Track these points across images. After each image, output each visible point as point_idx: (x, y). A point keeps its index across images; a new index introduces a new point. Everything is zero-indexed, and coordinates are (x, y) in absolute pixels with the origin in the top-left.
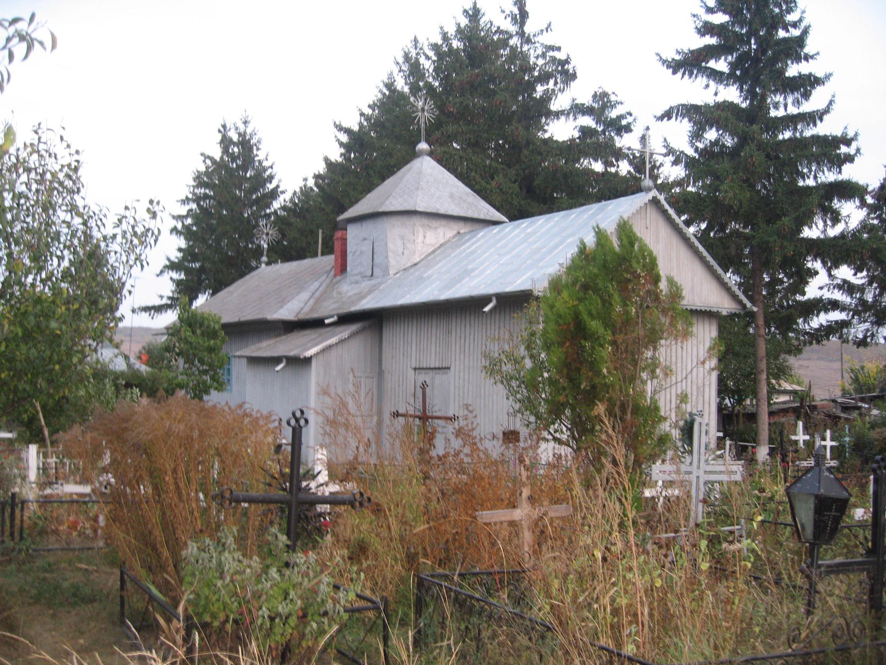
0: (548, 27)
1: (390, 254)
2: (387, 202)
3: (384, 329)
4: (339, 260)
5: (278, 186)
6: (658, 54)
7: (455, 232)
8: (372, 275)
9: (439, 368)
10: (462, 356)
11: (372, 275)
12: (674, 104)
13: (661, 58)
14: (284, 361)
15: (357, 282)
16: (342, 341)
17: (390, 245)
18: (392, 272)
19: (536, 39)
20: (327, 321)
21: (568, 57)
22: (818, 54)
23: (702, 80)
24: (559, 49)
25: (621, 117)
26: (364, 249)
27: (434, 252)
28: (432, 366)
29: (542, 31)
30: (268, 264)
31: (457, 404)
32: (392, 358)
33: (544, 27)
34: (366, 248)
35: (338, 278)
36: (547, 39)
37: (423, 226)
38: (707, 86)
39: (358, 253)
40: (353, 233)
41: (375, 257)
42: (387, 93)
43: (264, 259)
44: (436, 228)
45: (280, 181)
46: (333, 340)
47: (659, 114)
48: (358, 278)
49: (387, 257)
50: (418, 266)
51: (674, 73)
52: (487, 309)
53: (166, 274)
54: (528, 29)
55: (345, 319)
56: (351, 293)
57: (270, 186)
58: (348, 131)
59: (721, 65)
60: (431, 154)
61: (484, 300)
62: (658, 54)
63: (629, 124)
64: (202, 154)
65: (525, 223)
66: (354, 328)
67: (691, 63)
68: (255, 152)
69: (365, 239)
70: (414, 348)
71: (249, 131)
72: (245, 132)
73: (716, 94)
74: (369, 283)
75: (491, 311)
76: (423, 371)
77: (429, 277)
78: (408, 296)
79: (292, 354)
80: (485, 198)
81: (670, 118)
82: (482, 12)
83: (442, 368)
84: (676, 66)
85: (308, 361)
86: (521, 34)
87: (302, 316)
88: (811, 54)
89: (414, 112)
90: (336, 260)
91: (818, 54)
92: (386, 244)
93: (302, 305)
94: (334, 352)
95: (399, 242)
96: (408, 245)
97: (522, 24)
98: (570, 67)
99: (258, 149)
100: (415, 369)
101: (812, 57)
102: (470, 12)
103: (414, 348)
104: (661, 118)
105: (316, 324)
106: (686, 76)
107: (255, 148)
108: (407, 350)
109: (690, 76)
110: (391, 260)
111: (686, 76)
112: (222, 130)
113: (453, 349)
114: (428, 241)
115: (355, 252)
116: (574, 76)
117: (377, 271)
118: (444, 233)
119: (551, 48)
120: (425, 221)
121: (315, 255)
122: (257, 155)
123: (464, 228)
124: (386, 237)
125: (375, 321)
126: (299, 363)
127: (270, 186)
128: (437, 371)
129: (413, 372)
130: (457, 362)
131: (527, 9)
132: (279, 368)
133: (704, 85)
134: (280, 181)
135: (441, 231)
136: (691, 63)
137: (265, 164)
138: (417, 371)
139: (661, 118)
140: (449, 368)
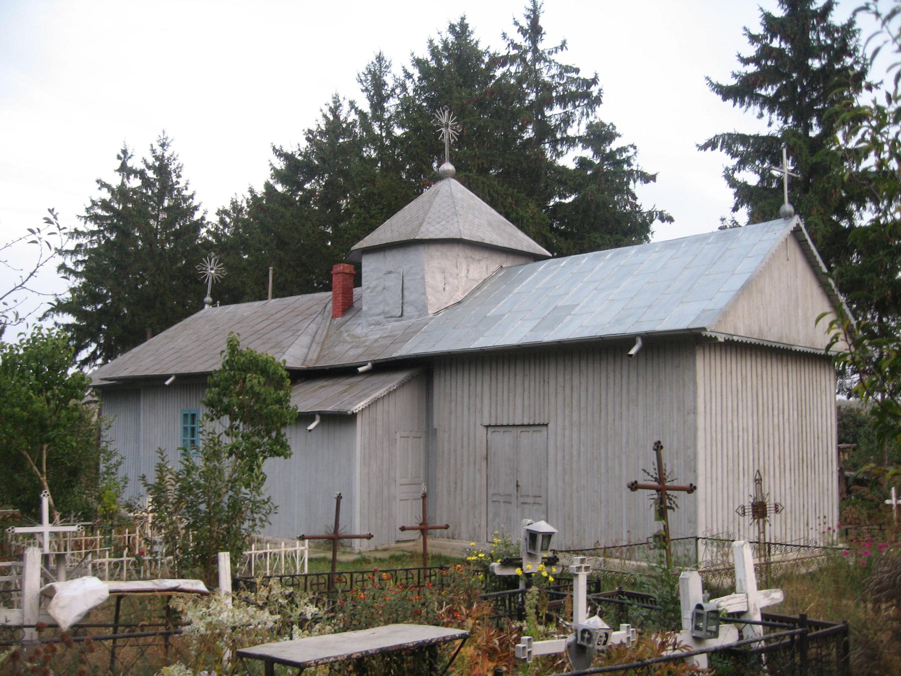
0: (563, 46)
1: (429, 290)
2: (423, 229)
3: (436, 382)
4: (340, 298)
5: (203, 218)
6: (707, 78)
7: (497, 266)
8: (402, 315)
9: (529, 425)
10: (567, 410)
11: (402, 315)
12: (719, 133)
13: (712, 83)
14: (318, 417)
15: (378, 323)
16: (389, 393)
17: (429, 279)
18: (431, 311)
19: (553, 57)
20: (360, 369)
21: (596, 77)
22: (881, 82)
23: (755, 109)
24: (577, 71)
25: (622, 150)
26: (388, 284)
27: (478, 288)
28: (526, 423)
29: (556, 48)
30: (213, 304)
31: (560, 468)
32: (451, 413)
33: (559, 44)
34: (393, 282)
35: (339, 320)
36: (562, 58)
37: (466, 258)
38: (761, 115)
39: (380, 288)
40: (372, 269)
41: (406, 293)
42: (331, 118)
43: (208, 299)
44: (479, 260)
45: (206, 213)
46: (381, 392)
47: (702, 143)
48: (380, 318)
49: (424, 294)
50: (466, 303)
51: (725, 99)
52: (633, 352)
53: (49, 318)
54: (541, 46)
55: (383, 367)
56: (372, 338)
57: (197, 216)
58: (288, 157)
59: (770, 91)
60: (456, 177)
61: (626, 342)
62: (707, 78)
63: (629, 158)
64: (98, 181)
65: (565, 261)
66: (400, 377)
67: (740, 92)
68: (175, 179)
69: (390, 272)
70: (486, 401)
71: (167, 155)
72: (163, 156)
73: (770, 124)
74: (398, 323)
75: (638, 353)
76: (502, 429)
77: (499, 317)
78: (481, 339)
79: (330, 408)
80: (522, 228)
81: (714, 148)
82: (470, 29)
83: (534, 425)
84: (726, 93)
85: (354, 416)
86: (535, 50)
87: (311, 365)
88: (874, 83)
89: (438, 127)
90: (335, 298)
91: (881, 82)
92: (423, 278)
93: (305, 350)
94: (380, 406)
95: (439, 277)
96: (450, 280)
97: (534, 42)
98: (594, 90)
99: (179, 176)
100: (487, 427)
101: (876, 86)
102: (458, 29)
103: (486, 401)
104: (704, 147)
105: (348, 371)
106: (738, 104)
107: (173, 175)
108: (467, 407)
109: (742, 104)
110: (429, 297)
111: (738, 104)
112: (122, 156)
113: (553, 400)
114: (471, 276)
115: (375, 288)
116: (598, 101)
117: (408, 310)
118: (480, 269)
119: (568, 69)
120: (469, 252)
121: (262, 297)
122: (178, 183)
123: (507, 262)
124: (423, 270)
125: (424, 370)
126: (341, 420)
127: (197, 216)
128: (523, 429)
129: (485, 430)
130: (560, 418)
131: (541, 23)
132: (311, 427)
133: (757, 114)
134: (206, 213)
135: (483, 264)
136: (740, 92)
137: (185, 193)
138: (490, 429)
139: (704, 147)
140: (547, 425)
